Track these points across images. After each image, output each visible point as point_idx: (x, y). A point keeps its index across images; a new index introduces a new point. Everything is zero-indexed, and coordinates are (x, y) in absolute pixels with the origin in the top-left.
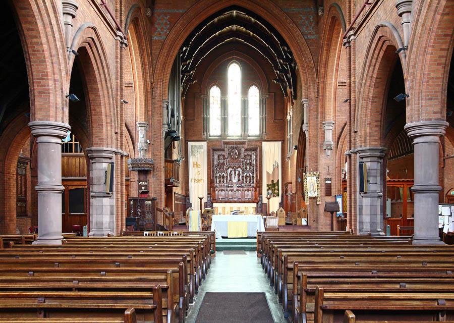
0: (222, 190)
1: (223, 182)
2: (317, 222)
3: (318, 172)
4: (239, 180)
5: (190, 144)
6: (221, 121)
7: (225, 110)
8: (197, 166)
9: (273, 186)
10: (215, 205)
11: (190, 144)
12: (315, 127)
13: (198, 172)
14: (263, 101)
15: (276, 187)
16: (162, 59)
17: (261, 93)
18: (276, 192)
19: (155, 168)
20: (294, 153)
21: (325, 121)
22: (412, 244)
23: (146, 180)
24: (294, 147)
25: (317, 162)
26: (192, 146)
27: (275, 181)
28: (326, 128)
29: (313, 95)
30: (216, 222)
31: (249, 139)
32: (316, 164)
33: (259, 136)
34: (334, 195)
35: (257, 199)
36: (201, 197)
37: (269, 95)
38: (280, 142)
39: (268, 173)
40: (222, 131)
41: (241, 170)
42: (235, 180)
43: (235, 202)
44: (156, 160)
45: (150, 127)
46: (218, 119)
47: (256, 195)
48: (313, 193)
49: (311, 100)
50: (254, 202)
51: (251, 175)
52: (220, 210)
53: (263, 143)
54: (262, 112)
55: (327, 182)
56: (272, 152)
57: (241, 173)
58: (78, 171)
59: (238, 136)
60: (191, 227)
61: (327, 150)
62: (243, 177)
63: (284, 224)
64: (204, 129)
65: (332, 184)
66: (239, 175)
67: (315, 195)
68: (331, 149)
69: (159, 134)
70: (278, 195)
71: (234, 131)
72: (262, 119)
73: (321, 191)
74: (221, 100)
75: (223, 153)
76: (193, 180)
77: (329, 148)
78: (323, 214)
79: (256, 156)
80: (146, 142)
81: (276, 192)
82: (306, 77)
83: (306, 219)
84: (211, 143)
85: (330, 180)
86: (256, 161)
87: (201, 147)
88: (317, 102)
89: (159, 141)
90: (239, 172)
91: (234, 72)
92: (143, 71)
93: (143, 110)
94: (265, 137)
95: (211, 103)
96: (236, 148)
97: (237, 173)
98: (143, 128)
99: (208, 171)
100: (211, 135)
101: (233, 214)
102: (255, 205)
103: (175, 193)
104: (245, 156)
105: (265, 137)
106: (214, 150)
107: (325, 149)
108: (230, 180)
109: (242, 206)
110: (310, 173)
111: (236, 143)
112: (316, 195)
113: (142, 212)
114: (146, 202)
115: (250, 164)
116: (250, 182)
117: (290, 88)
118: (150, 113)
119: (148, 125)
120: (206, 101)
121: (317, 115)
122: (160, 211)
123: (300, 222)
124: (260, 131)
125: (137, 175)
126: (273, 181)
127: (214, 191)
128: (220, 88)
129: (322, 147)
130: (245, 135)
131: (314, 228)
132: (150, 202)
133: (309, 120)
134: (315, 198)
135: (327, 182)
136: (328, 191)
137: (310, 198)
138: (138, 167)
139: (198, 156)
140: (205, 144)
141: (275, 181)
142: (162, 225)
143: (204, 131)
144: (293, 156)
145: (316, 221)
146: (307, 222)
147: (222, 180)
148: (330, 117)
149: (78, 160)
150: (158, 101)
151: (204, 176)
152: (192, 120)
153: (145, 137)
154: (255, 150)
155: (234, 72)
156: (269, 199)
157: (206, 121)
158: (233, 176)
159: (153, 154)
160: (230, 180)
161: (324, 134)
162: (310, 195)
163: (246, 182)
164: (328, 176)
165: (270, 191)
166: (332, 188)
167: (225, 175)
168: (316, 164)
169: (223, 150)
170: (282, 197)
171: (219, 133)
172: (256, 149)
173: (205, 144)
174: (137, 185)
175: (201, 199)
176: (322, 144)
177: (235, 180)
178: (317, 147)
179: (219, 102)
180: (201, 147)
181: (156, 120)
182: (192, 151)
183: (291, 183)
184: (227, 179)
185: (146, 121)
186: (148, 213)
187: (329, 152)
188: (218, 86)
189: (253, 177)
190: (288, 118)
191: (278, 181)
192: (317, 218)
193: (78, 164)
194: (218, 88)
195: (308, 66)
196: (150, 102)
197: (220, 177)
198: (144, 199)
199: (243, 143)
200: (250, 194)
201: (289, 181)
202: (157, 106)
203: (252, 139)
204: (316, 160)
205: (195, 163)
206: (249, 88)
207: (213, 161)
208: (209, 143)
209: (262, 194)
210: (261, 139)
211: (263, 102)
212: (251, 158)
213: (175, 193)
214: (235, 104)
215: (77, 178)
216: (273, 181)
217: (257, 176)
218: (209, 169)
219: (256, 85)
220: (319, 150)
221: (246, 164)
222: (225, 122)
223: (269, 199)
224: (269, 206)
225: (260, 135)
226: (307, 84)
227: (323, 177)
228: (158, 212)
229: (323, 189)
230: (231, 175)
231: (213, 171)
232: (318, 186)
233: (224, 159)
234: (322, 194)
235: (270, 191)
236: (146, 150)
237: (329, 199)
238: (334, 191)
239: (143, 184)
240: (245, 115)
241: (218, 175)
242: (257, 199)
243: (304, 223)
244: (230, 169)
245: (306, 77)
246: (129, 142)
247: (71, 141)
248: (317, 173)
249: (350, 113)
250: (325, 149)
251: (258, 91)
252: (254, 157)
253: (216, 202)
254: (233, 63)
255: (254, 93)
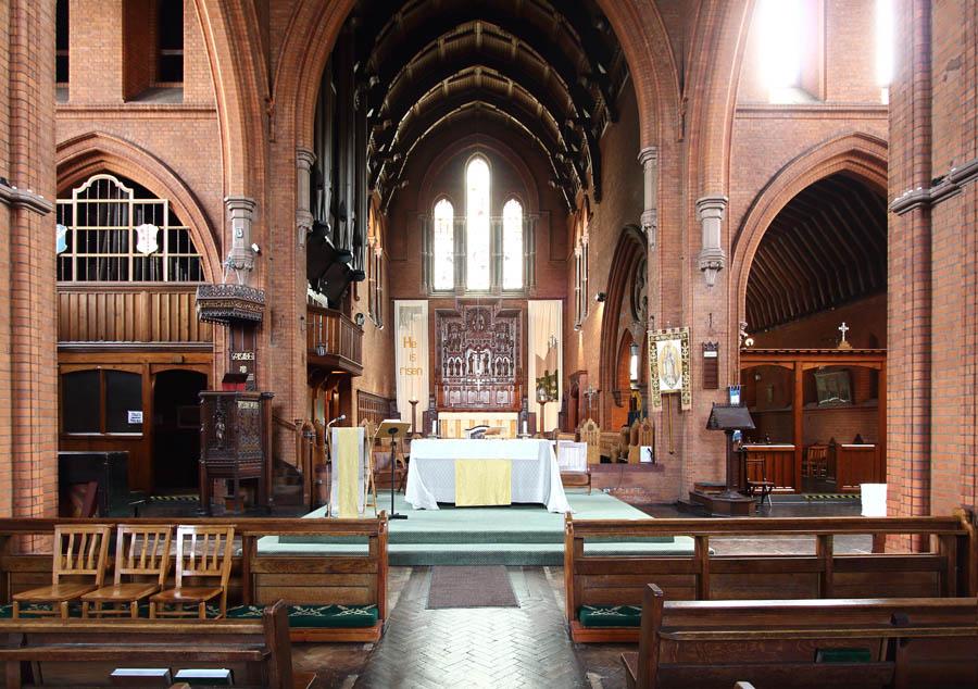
0: (455, 389)
1: (458, 373)
2: (680, 455)
3: (686, 330)
4: (487, 371)
5: (398, 304)
6: (455, 263)
7: (461, 242)
8: (411, 345)
9: (547, 382)
10: (442, 416)
11: (398, 304)
12: (676, 217)
13: (412, 356)
14: (529, 227)
15: (554, 384)
16: (295, 42)
17: (526, 212)
18: (553, 392)
19: (278, 318)
20: (595, 311)
21: (703, 195)
22: (929, 515)
23: (250, 348)
24: (597, 297)
25: (679, 305)
26: (401, 309)
27: (552, 373)
28: (706, 213)
29: (669, 135)
30: (421, 460)
31: (504, 296)
32: (677, 310)
33: (522, 291)
34: (724, 388)
35: (519, 406)
36: (414, 399)
37: (541, 215)
38: (561, 302)
39: (538, 358)
40: (455, 282)
41: (489, 353)
42: (479, 371)
43: (479, 411)
44: (277, 298)
45: (260, 211)
46: (448, 258)
47: (517, 398)
48: (671, 381)
49: (665, 146)
50: (513, 411)
51: (508, 361)
52: (451, 425)
53: (530, 302)
54: (527, 247)
55: (707, 354)
56: (545, 318)
57: (490, 358)
58: (83, 327)
59: (485, 291)
60: (336, 479)
61: (707, 270)
62: (493, 364)
63: (599, 460)
64: (423, 277)
65: (720, 360)
66: (486, 361)
67: (678, 386)
68: (719, 269)
69: (288, 233)
70: (557, 398)
71: (478, 282)
72: (527, 260)
73: (692, 378)
74: (455, 226)
75: (456, 320)
76: (404, 371)
77: (713, 264)
78: (696, 436)
79: (518, 326)
80: (251, 250)
81: (553, 392)
82: (654, 91)
83: (650, 448)
84: (436, 303)
85: (715, 348)
86: (518, 335)
87: (418, 310)
88: (681, 152)
89: (287, 250)
90: (487, 355)
91: (478, 175)
92: (234, 54)
93: (241, 164)
94: (533, 292)
95: (436, 228)
96: (481, 311)
97: (483, 357)
98: (241, 213)
99: (430, 351)
100: (436, 288)
101: (473, 436)
102: (515, 416)
103: (358, 391)
104: (498, 326)
105: (533, 292)
106: (443, 315)
107: (703, 270)
108: (471, 371)
109: (493, 419)
110: (665, 332)
111: (482, 302)
112: (681, 388)
113: (229, 432)
114: (240, 403)
115: (507, 341)
116: (506, 374)
117: (585, 186)
118: (261, 176)
119: (256, 203)
120: (428, 229)
121: (680, 185)
122: (290, 428)
123: (635, 455)
124: (524, 281)
125: (228, 336)
126: (547, 372)
127: (441, 390)
128: (452, 203)
129: (694, 265)
130: (496, 289)
131: (672, 469)
132: (254, 405)
133: (660, 198)
134: (678, 394)
135: (707, 354)
136: (710, 377)
137: (665, 395)
138: (217, 309)
139: (413, 326)
140: (424, 304)
141: (552, 373)
142: (293, 463)
143: (423, 281)
144: (591, 320)
145: (677, 452)
146: (653, 454)
147: (455, 370)
148: (716, 187)
149: (120, 298)
150: (285, 149)
151: (423, 363)
152: (401, 261)
153: (247, 236)
154: (514, 314)
155: (478, 175)
156: (543, 403)
157: (426, 263)
158: (475, 363)
159: (270, 283)
160: (471, 371)
161: (699, 232)
162: (664, 387)
163: (499, 374)
164: (710, 339)
165: (542, 391)
166: (720, 367)
167: (461, 361)
168: (677, 310)
169: (458, 316)
170: (564, 400)
171: (450, 285)
172: (514, 313)
173: (424, 304)
174: (228, 360)
175: (414, 404)
176: (695, 257)
177: (479, 371)
178: (680, 266)
179: (451, 229)
180: (418, 310)
181: (280, 198)
182: (401, 318)
183: (586, 372)
184: (464, 370)
185: (247, 193)
186: (247, 434)
187: (711, 277)
188: (448, 199)
189: (512, 365)
190: (578, 251)
191: (556, 371)
192: (680, 446)
193: (83, 307)
194: (449, 204)
195: (659, 63)
196: (260, 145)
197: (451, 365)
198: (233, 396)
199: (493, 302)
200: (505, 397)
201: (580, 368)
202: (282, 161)
203: (509, 295)
204: (677, 298)
205: (407, 340)
206: (504, 204)
207: (440, 336)
208: (432, 301)
209: (527, 397)
210: (526, 296)
211: (529, 229)
212: (507, 331)
213: (358, 391)
214: (478, 232)
215: (83, 344)
216: (547, 372)
217: (518, 363)
218: (431, 350)
219: (517, 199)
220: (687, 276)
221: (499, 340)
222: (461, 265)
223: (543, 403)
224: (542, 419)
225: (524, 288)
226: (655, 109)
227: (699, 339)
228: (286, 430)
229: (698, 371)
230: (471, 361)
231: (439, 354)
232: (684, 363)
233: (460, 331)
234: (696, 385)
235: (542, 391)
236: (250, 270)
237: (709, 399)
238: (726, 376)
239: (244, 358)
240: (497, 252)
241: (449, 361)
242: (519, 406)
243: (645, 456)
244: (470, 351)
245: (654, 91)
246: (211, 252)
247: (69, 250)
248: (681, 330)
249: (847, 111)
250: (703, 270)
251: (521, 209)
252: (515, 326)
253: (445, 411)
254: (474, 158)
255: (514, 211)
